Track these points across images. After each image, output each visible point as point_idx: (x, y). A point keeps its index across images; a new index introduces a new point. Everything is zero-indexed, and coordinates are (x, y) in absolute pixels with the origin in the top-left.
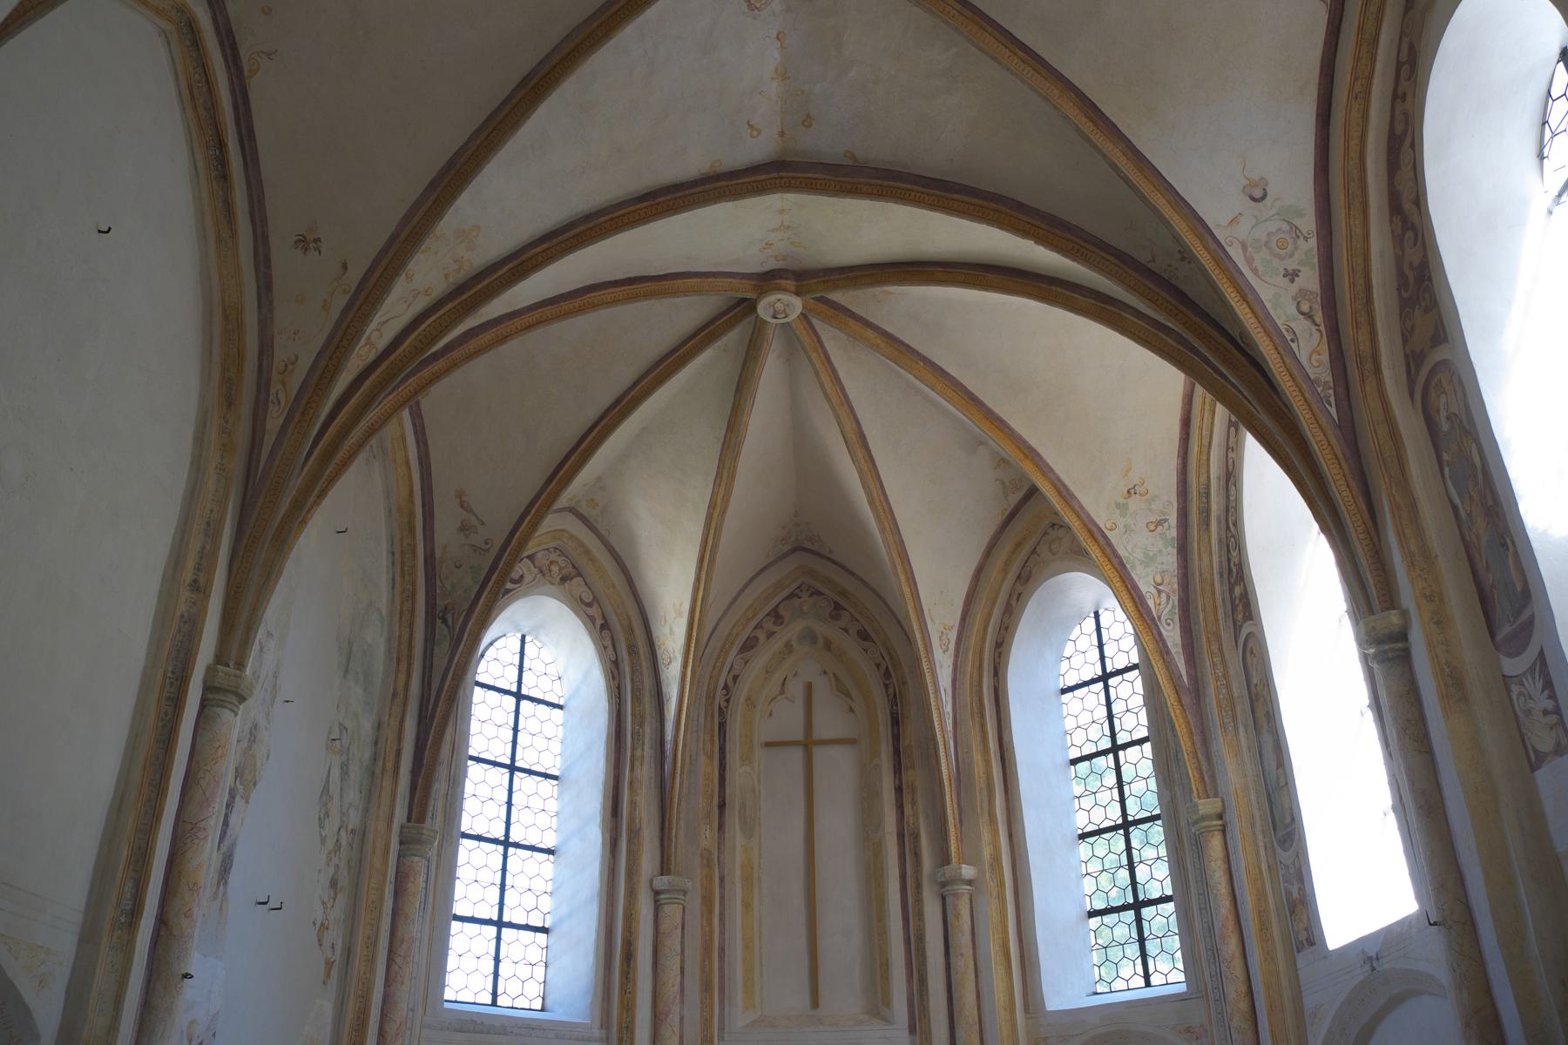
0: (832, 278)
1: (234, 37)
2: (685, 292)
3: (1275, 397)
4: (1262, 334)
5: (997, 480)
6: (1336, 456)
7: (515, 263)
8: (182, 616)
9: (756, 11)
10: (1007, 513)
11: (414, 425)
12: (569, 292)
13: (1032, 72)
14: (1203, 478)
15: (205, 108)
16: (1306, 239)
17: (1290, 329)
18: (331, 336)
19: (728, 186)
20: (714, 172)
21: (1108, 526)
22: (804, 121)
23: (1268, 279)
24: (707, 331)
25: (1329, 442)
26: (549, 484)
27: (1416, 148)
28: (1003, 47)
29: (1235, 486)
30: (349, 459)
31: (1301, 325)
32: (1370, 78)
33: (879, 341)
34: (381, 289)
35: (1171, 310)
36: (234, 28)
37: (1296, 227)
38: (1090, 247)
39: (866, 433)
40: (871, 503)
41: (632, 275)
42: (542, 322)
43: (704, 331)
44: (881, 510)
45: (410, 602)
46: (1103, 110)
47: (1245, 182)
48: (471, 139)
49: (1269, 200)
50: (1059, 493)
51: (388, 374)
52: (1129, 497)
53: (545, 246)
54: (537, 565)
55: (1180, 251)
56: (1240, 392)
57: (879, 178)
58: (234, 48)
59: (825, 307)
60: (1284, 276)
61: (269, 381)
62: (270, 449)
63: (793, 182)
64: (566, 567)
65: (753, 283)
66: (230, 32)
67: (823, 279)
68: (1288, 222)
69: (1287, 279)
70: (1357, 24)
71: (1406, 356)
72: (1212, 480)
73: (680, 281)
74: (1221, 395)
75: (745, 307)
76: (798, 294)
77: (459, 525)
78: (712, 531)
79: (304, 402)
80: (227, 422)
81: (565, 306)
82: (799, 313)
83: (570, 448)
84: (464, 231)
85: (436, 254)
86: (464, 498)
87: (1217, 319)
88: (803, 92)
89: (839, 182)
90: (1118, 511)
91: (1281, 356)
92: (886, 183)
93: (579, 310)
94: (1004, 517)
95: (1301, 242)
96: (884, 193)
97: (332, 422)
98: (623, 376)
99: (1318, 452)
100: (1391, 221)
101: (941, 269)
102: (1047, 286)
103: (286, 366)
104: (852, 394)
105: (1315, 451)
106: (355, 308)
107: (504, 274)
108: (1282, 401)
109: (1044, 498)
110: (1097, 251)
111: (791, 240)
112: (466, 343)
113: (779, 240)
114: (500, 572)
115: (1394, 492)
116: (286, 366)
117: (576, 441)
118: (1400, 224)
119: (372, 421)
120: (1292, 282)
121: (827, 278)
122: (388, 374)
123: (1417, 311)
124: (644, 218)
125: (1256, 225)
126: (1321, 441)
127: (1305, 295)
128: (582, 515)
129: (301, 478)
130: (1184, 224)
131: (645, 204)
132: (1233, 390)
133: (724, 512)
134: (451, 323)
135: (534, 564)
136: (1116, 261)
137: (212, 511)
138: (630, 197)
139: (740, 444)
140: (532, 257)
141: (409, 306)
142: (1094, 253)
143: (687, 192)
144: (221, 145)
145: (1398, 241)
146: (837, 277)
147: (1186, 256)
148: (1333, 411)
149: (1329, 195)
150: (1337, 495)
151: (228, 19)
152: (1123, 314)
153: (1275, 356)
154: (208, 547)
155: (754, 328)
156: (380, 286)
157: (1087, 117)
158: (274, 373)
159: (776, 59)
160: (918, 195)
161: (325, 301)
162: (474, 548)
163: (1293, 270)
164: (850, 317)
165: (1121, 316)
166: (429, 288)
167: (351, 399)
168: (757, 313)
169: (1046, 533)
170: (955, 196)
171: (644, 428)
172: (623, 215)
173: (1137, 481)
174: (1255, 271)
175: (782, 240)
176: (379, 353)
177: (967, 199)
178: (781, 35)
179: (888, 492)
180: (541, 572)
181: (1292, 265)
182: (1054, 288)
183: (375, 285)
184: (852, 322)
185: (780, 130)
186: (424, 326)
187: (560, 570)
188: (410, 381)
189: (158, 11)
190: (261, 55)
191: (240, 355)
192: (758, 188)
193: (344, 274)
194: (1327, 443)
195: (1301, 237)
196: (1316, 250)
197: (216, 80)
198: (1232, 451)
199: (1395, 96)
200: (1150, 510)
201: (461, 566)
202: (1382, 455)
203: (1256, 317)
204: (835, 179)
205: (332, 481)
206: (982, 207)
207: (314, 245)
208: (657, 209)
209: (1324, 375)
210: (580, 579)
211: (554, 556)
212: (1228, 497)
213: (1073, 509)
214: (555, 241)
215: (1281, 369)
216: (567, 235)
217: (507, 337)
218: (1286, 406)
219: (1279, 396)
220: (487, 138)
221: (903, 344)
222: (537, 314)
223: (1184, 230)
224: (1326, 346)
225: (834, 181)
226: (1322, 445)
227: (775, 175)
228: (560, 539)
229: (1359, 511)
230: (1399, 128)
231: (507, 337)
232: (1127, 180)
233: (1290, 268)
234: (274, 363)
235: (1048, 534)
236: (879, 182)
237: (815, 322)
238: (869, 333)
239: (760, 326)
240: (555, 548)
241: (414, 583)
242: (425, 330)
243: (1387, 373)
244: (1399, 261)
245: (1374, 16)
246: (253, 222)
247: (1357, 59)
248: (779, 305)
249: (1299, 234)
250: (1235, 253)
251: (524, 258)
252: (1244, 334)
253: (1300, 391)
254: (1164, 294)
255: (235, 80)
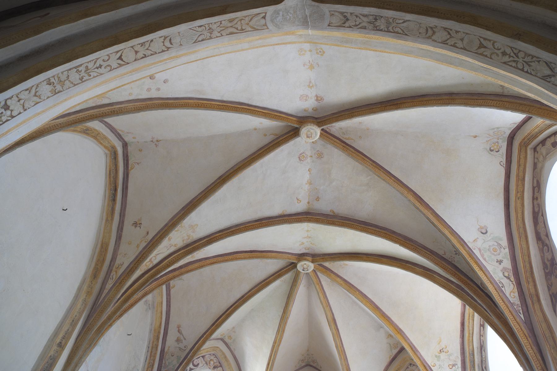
0: (325, 257)
1: (128, 158)
2: (271, 258)
3: (497, 309)
4: (490, 283)
5: (387, 343)
6: (525, 335)
7: (209, 239)
8: (51, 356)
9: (302, 161)
10: (392, 357)
11: (167, 298)
12: (228, 253)
13: (397, 185)
14: (471, 347)
15: (113, 178)
16: (504, 249)
17: (501, 282)
18: (137, 257)
19: (288, 219)
20: (283, 214)
21: (432, 365)
22: (317, 199)
23: (490, 262)
24: (278, 273)
25: (521, 328)
26: (212, 326)
27: (544, 216)
28: (387, 176)
29: (484, 351)
30: (135, 303)
31: (505, 281)
32: (523, 192)
33: (342, 282)
34: (158, 242)
35: (452, 273)
36: (129, 155)
37: (500, 244)
38: (420, 248)
39: (336, 318)
40: (337, 347)
41: (252, 249)
42: (217, 262)
43: (277, 273)
44: (340, 351)
45: (151, 368)
46: (424, 199)
47: (479, 227)
48: (199, 194)
49: (488, 234)
50: (412, 349)
51: (155, 273)
52: (441, 353)
53: (220, 234)
54: (205, 360)
55: (455, 251)
56: (483, 307)
57: (342, 220)
58: (128, 161)
59: (322, 268)
60: (497, 262)
61: (112, 270)
62: (105, 295)
63: (311, 219)
64: (216, 362)
65: (296, 257)
66: (127, 156)
67: (322, 257)
68: (497, 242)
69: (498, 263)
70: (516, 173)
71: (550, 296)
72: (475, 348)
73: (269, 254)
74: (475, 309)
75: (292, 266)
76: (312, 262)
77: (176, 339)
78: (274, 352)
79: (121, 279)
80: (92, 283)
81: (226, 258)
82: (312, 269)
83: (223, 312)
84: (192, 225)
85: (181, 232)
86: (180, 329)
87: (471, 277)
88: (317, 189)
89: (328, 220)
90: (436, 359)
91: (498, 292)
92: (344, 222)
93: (231, 260)
94: (391, 359)
95: (502, 249)
96: (344, 225)
97: (131, 288)
98: (246, 288)
99: (517, 333)
100: (538, 243)
101: (365, 256)
102: (405, 264)
103: (119, 266)
104: (331, 303)
105: (515, 332)
106: (148, 248)
107: (204, 242)
108: (500, 311)
109: (407, 353)
110: (424, 250)
111: (311, 242)
112: (187, 266)
113: (306, 242)
114: (188, 360)
115: (552, 352)
116: (119, 266)
117: (225, 310)
118: (541, 244)
119: (146, 290)
120: (500, 265)
121: (323, 257)
122: (155, 273)
123: (552, 277)
124: (257, 227)
125: (484, 242)
126: (518, 328)
127: (506, 270)
128: (225, 342)
129: (114, 308)
130: (456, 241)
131: (258, 223)
132: (480, 307)
133: (279, 345)
134: (182, 257)
135: (204, 360)
136: (430, 254)
137: (76, 316)
138: (252, 220)
139: (287, 318)
140: (215, 237)
141: (168, 249)
142: (422, 250)
143: (273, 220)
144: (116, 190)
145: (541, 251)
146: (327, 257)
147: (457, 253)
148: (522, 316)
149: (512, 233)
150: (528, 352)
151: (128, 152)
152: (434, 275)
153: (496, 292)
154: (70, 330)
155: (296, 274)
156: (158, 241)
157: (417, 201)
158: (114, 268)
159: (307, 177)
160: (356, 226)
161: (138, 244)
162: (180, 349)
163: (500, 260)
164: (331, 273)
165: (434, 276)
166: (176, 244)
167: (139, 280)
168: (297, 268)
169: (408, 368)
170: (370, 227)
171: (252, 309)
172: (249, 226)
173: (443, 346)
174: (485, 259)
175: (308, 242)
176: (153, 265)
177: (374, 229)
178: (310, 170)
179: (344, 344)
180: (206, 363)
181: (500, 258)
182: (407, 265)
183: (156, 240)
184: (332, 274)
185: (308, 201)
186: (172, 257)
187: (213, 364)
188: (164, 277)
189: (106, 147)
190: (136, 163)
191: (104, 260)
192: (298, 220)
193: (147, 236)
194: (521, 329)
195: (502, 248)
196: (508, 253)
197: (119, 169)
198: (482, 336)
199: (533, 199)
200: (450, 359)
201: (173, 356)
202: (545, 336)
203: (486, 277)
204: (327, 219)
205: (125, 311)
206: (380, 232)
207: (139, 225)
208: (262, 225)
209: (517, 301)
210: (221, 368)
211: (212, 358)
212: (482, 356)
213: (418, 356)
214: (224, 232)
215: (499, 298)
216: (228, 231)
217: (203, 266)
218: (502, 313)
219: (499, 309)
220: (204, 195)
221: (351, 284)
222: (215, 260)
223: (456, 243)
224: (516, 290)
225: (326, 220)
226: (519, 330)
227: (305, 216)
228: (216, 351)
229: (538, 359)
230: (536, 210)
231: (203, 266)
232: (432, 223)
233: (499, 259)
234: (115, 264)
235: (409, 368)
236: (342, 221)
237: (319, 274)
238: (338, 279)
239: (298, 274)
240: (214, 354)
241: (154, 361)
242: (172, 259)
243: (543, 302)
244: (543, 258)
245: (522, 171)
246: (120, 216)
247: (517, 186)
248: (305, 266)
249: (501, 247)
250: (476, 252)
251: (212, 237)
252: (482, 283)
253: (507, 307)
254: (450, 267)
255: (125, 170)
